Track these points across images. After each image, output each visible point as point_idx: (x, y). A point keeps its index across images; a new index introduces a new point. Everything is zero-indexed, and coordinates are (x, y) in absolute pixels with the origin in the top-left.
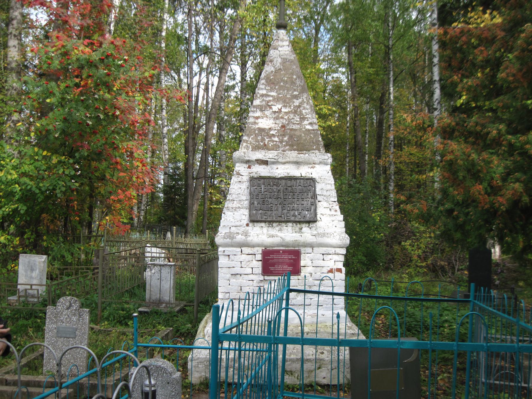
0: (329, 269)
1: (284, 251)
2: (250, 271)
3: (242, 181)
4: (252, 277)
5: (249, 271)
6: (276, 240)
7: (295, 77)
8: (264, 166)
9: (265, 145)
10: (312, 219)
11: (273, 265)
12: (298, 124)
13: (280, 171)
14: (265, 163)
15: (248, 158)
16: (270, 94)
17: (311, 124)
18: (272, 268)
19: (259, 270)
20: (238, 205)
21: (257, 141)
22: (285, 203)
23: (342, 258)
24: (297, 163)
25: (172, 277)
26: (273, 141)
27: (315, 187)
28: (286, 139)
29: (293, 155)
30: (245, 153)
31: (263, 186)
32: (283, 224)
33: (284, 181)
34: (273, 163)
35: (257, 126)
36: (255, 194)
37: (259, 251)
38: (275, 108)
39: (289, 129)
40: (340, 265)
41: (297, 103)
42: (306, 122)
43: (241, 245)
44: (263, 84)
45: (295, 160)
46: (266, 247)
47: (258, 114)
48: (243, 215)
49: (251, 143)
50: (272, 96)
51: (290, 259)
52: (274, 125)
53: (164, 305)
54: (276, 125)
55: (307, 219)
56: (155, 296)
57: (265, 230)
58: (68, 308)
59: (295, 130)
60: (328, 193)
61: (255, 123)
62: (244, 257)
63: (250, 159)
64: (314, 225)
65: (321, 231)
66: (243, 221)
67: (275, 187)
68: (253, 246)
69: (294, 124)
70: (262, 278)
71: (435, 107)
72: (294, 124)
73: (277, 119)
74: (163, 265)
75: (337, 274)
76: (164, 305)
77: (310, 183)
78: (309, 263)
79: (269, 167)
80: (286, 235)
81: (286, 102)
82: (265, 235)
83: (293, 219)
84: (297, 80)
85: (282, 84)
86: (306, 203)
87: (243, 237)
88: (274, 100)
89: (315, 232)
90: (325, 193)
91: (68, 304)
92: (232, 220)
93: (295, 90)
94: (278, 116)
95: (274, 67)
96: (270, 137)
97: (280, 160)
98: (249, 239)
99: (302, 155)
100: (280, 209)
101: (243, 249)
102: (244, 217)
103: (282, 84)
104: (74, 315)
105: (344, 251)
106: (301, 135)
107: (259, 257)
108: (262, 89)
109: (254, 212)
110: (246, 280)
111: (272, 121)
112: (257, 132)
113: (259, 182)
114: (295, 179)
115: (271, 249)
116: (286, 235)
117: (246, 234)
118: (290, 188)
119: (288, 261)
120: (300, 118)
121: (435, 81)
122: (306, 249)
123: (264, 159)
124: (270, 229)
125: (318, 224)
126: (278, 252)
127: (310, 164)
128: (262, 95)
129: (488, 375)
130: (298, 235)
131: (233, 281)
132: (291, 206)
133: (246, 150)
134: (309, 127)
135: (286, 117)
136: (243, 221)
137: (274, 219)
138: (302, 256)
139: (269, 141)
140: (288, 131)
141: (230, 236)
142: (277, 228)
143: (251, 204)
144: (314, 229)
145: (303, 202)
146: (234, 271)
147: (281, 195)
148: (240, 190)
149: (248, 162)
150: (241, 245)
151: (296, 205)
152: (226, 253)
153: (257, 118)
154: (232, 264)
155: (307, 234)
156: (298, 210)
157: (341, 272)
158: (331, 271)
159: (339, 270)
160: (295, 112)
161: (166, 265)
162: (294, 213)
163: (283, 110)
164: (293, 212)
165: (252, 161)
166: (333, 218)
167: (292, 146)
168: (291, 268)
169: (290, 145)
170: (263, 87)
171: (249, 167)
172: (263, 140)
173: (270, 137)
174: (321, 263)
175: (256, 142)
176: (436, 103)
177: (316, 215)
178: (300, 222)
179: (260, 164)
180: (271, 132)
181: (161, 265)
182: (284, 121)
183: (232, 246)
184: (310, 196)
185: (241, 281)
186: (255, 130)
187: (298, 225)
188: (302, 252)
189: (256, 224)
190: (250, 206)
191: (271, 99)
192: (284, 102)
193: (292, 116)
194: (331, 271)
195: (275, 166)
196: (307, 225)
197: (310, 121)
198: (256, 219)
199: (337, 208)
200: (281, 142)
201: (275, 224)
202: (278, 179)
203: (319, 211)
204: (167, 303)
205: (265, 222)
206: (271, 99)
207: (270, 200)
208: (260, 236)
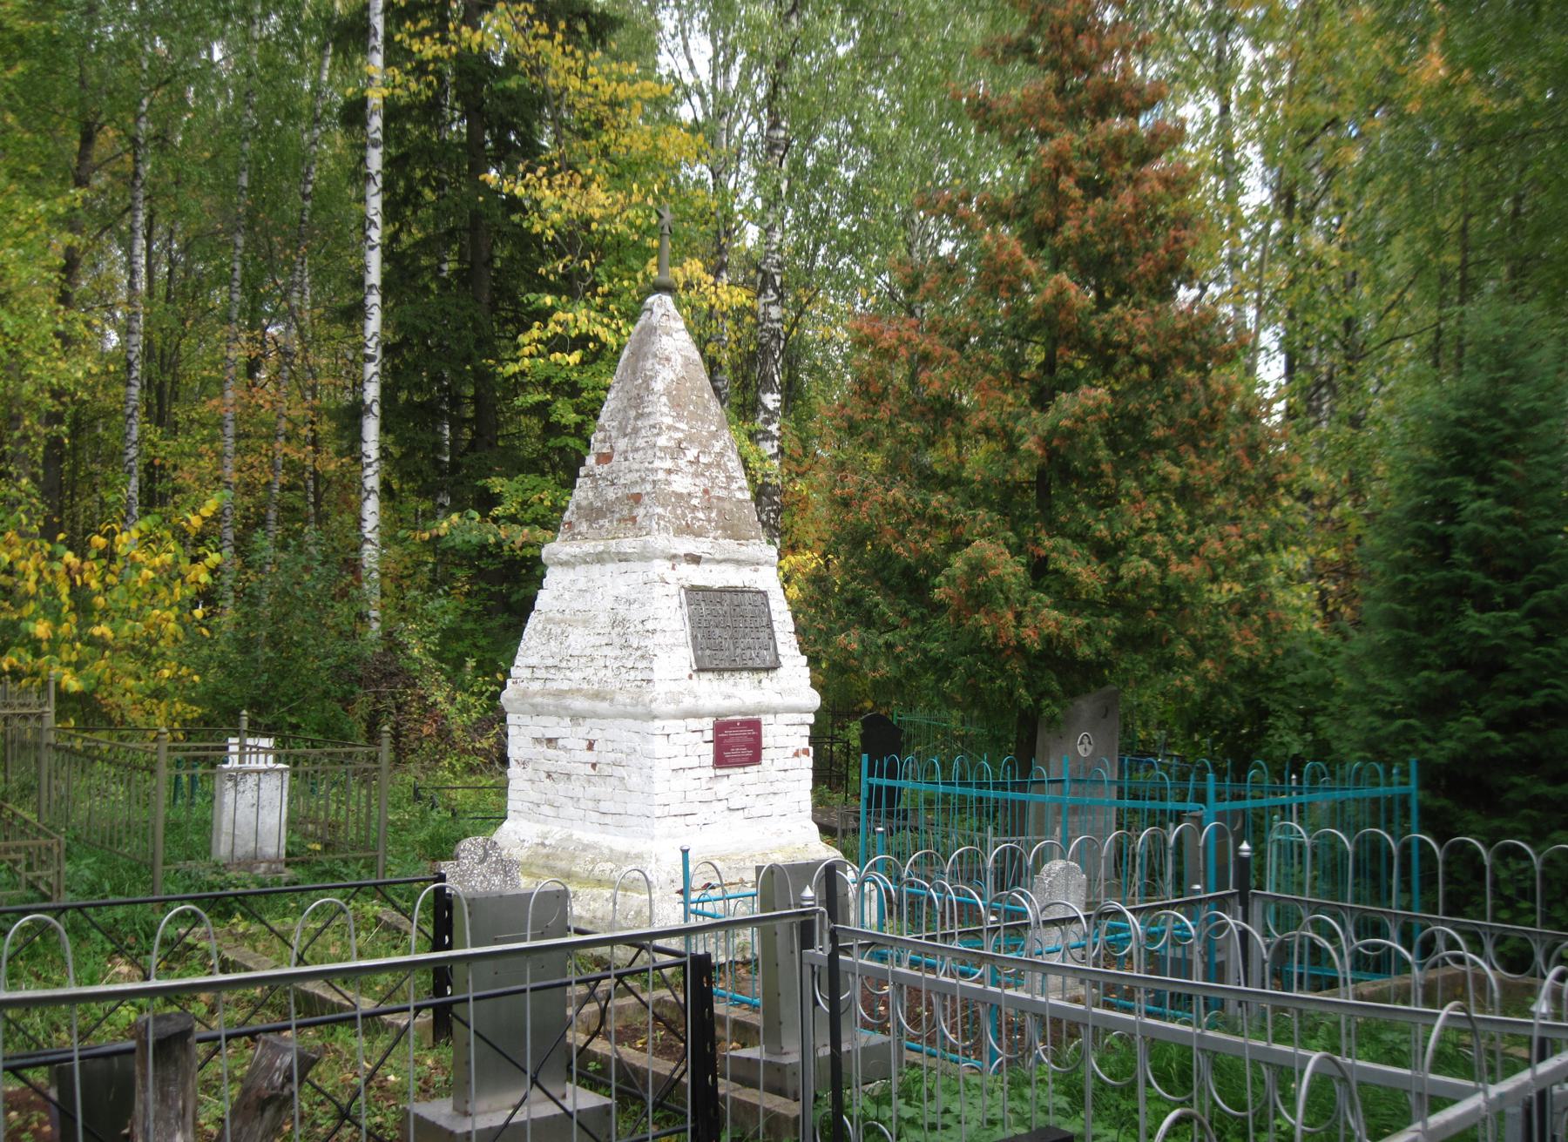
1: (743, 723)
8: (694, 566)
14: (695, 559)
15: (673, 551)
18: (727, 755)
19: (709, 759)
20: (672, 641)
23: (807, 731)
25: (285, 799)
34: (708, 561)
37: (708, 724)
40: (805, 743)
46: (718, 716)
47: (668, 464)
53: (264, 866)
56: (245, 846)
57: (715, 683)
58: (482, 861)
61: (668, 483)
70: (712, 772)
71: (369, 352)
74: (265, 772)
75: (804, 757)
76: (264, 866)
80: (737, 694)
83: (750, 664)
89: (778, 688)
91: (480, 852)
98: (700, 702)
104: (495, 872)
105: (811, 719)
107: (709, 735)
111: (689, 480)
114: (735, 591)
116: (737, 694)
121: (372, 286)
125: (780, 671)
126: (734, 723)
128: (669, 428)
130: (757, 692)
134: (739, 495)
138: (764, 729)
142: (731, 681)
143: (694, 638)
146: (676, 764)
153: (669, 472)
159: (806, 752)
161: (271, 770)
167: (724, 529)
172: (684, 516)
176: (371, 344)
177: (777, 656)
179: (688, 562)
181: (258, 772)
194: (796, 754)
199: (795, 642)
201: (726, 675)
204: (271, 862)
205: (713, 670)
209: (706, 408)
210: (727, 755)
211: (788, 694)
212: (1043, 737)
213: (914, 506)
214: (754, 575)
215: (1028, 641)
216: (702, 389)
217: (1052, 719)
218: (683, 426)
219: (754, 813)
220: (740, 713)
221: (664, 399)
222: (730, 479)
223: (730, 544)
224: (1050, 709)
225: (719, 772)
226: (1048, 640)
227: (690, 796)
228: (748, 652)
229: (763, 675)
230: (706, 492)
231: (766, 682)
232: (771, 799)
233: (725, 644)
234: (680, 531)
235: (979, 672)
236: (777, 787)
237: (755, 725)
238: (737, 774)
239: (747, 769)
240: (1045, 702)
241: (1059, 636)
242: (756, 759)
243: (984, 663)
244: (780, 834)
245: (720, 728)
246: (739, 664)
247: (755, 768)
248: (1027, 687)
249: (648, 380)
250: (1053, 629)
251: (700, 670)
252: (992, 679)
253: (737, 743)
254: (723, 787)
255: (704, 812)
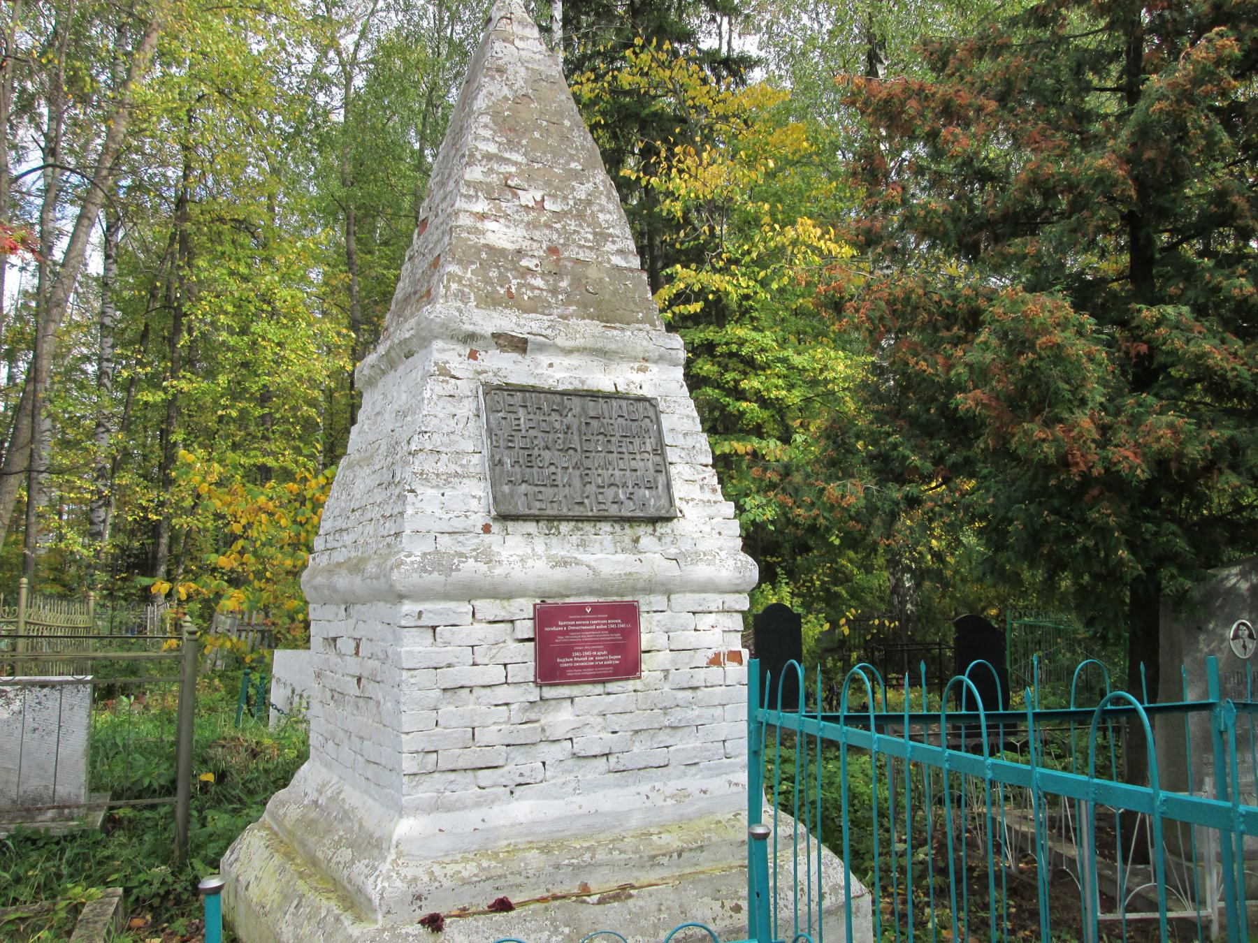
0: (710, 654)
1: (597, 609)
2: (497, 674)
3: (457, 393)
4: (503, 694)
5: (497, 674)
6: (578, 574)
7: (567, 123)
8: (515, 356)
9: (510, 295)
10: (663, 513)
11: (567, 651)
12: (590, 248)
13: (557, 372)
14: (520, 346)
15: (468, 328)
16: (507, 155)
17: (620, 252)
18: (564, 662)
19: (528, 671)
20: (453, 468)
21: (488, 281)
22: (587, 463)
23: (737, 622)
24: (603, 354)
26: (533, 288)
27: (659, 423)
28: (564, 284)
29: (588, 330)
30: (460, 310)
31: (521, 413)
32: (588, 527)
33: (576, 400)
34: (541, 348)
35: (482, 241)
36: (504, 433)
37: (524, 608)
38: (527, 198)
39: (569, 259)
40: (736, 643)
41: (581, 192)
42: (609, 247)
43: (469, 592)
44: (486, 126)
45: (599, 345)
46: (544, 597)
47: (481, 206)
48: (474, 497)
49: (470, 286)
50: (515, 163)
51: (612, 631)
52: (528, 243)
54: (535, 245)
55: (652, 512)
57: (539, 545)
59: (585, 263)
60: (690, 442)
62: (481, 630)
63: (478, 330)
64: (662, 528)
65: (686, 546)
66: (473, 517)
67: (555, 416)
68: (509, 596)
69: (581, 247)
70: (534, 694)
72: (581, 247)
73: (535, 228)
75: (731, 667)
77: (644, 409)
78: (662, 641)
79: (528, 359)
80: (599, 559)
81: (556, 189)
82: (533, 560)
83: (613, 510)
84: (576, 133)
85: (537, 135)
86: (645, 464)
87: (482, 567)
88: (519, 175)
89: (673, 551)
90: (680, 441)
92: (439, 513)
93: (572, 158)
94: (537, 220)
95: (511, 87)
96: (523, 276)
97: (560, 341)
99: (615, 332)
100: (577, 482)
101: (477, 603)
102: (474, 504)
103: (537, 135)
106: (601, 280)
107: (526, 628)
108: (485, 139)
109: (506, 489)
110: (489, 705)
111: (521, 232)
112: (484, 255)
113: (510, 400)
115: (559, 601)
116: (599, 559)
117: (486, 556)
118: (594, 423)
119: (606, 636)
120: (595, 234)
122: (652, 598)
123: (518, 332)
124: (554, 540)
126: (579, 609)
127: (635, 359)
128: (489, 157)
129: (1108, 903)
130: (632, 557)
131: (447, 709)
132: (606, 474)
133: (459, 304)
134: (617, 260)
135: (558, 226)
136: (473, 517)
137: (565, 511)
138: (644, 622)
139: (520, 286)
140: (569, 265)
141: (438, 562)
142: (574, 539)
143: (496, 464)
144: (668, 540)
145: (633, 464)
147: (576, 443)
148: (452, 422)
149: (470, 338)
150: (469, 592)
151: (617, 473)
152: (426, 621)
153: (483, 217)
154: (443, 654)
155: (650, 556)
156: (625, 485)
157: (741, 662)
158: (715, 661)
159: (735, 657)
160: (580, 216)
162: (617, 495)
163: (548, 205)
164: (614, 489)
165: (483, 337)
166: (712, 511)
167: (583, 305)
168: (615, 659)
169: (578, 303)
170: (487, 133)
171: (473, 355)
172: (503, 280)
173: (523, 276)
174: (690, 639)
175: (486, 283)
178: (631, 520)
179: (502, 348)
180: (524, 263)
182: (555, 237)
183: (446, 597)
184: (649, 448)
185: (472, 707)
186: (480, 251)
187: (628, 530)
188: (643, 608)
189: (510, 524)
190: (492, 469)
191: (513, 169)
192: (548, 183)
193: (572, 225)
194: (715, 661)
195: (544, 359)
196: (650, 529)
197: (619, 246)
198: (513, 512)
200: (554, 291)
201: (565, 527)
202: (563, 393)
203: (679, 490)
205: (537, 519)
206: (513, 169)
207: (547, 455)
208: (530, 563)
209: (564, 138)
210: (564, 662)
211: (696, 560)
212: (1167, 629)
213: (938, 303)
214: (638, 377)
215: (1124, 466)
216: (561, 114)
217: (1182, 598)
218: (515, 157)
219: (626, 761)
220: (592, 592)
221: (486, 119)
222: (602, 236)
223: (595, 327)
224: (1171, 581)
225: (549, 692)
226: (1161, 463)
227: (484, 736)
228: (610, 493)
229: (642, 530)
230: (553, 250)
231: (647, 541)
232: (664, 737)
233: (561, 478)
234: (490, 301)
235: (1046, 525)
236: (675, 717)
237: (629, 613)
238: (590, 698)
239: (611, 687)
240: (1165, 573)
241: (1180, 455)
242: (629, 668)
243: (1054, 511)
244: (681, 796)
245: (545, 616)
246: (591, 509)
247: (631, 685)
248: (1131, 547)
249: (916, 467)
250: (1167, 439)
251: (504, 517)
252: (1069, 538)
253: (583, 643)
254: (562, 718)
255: (522, 764)
